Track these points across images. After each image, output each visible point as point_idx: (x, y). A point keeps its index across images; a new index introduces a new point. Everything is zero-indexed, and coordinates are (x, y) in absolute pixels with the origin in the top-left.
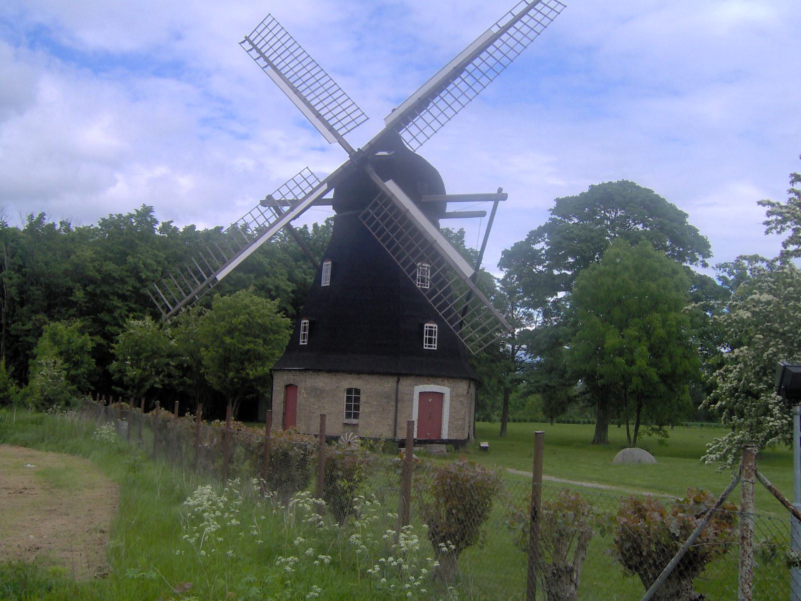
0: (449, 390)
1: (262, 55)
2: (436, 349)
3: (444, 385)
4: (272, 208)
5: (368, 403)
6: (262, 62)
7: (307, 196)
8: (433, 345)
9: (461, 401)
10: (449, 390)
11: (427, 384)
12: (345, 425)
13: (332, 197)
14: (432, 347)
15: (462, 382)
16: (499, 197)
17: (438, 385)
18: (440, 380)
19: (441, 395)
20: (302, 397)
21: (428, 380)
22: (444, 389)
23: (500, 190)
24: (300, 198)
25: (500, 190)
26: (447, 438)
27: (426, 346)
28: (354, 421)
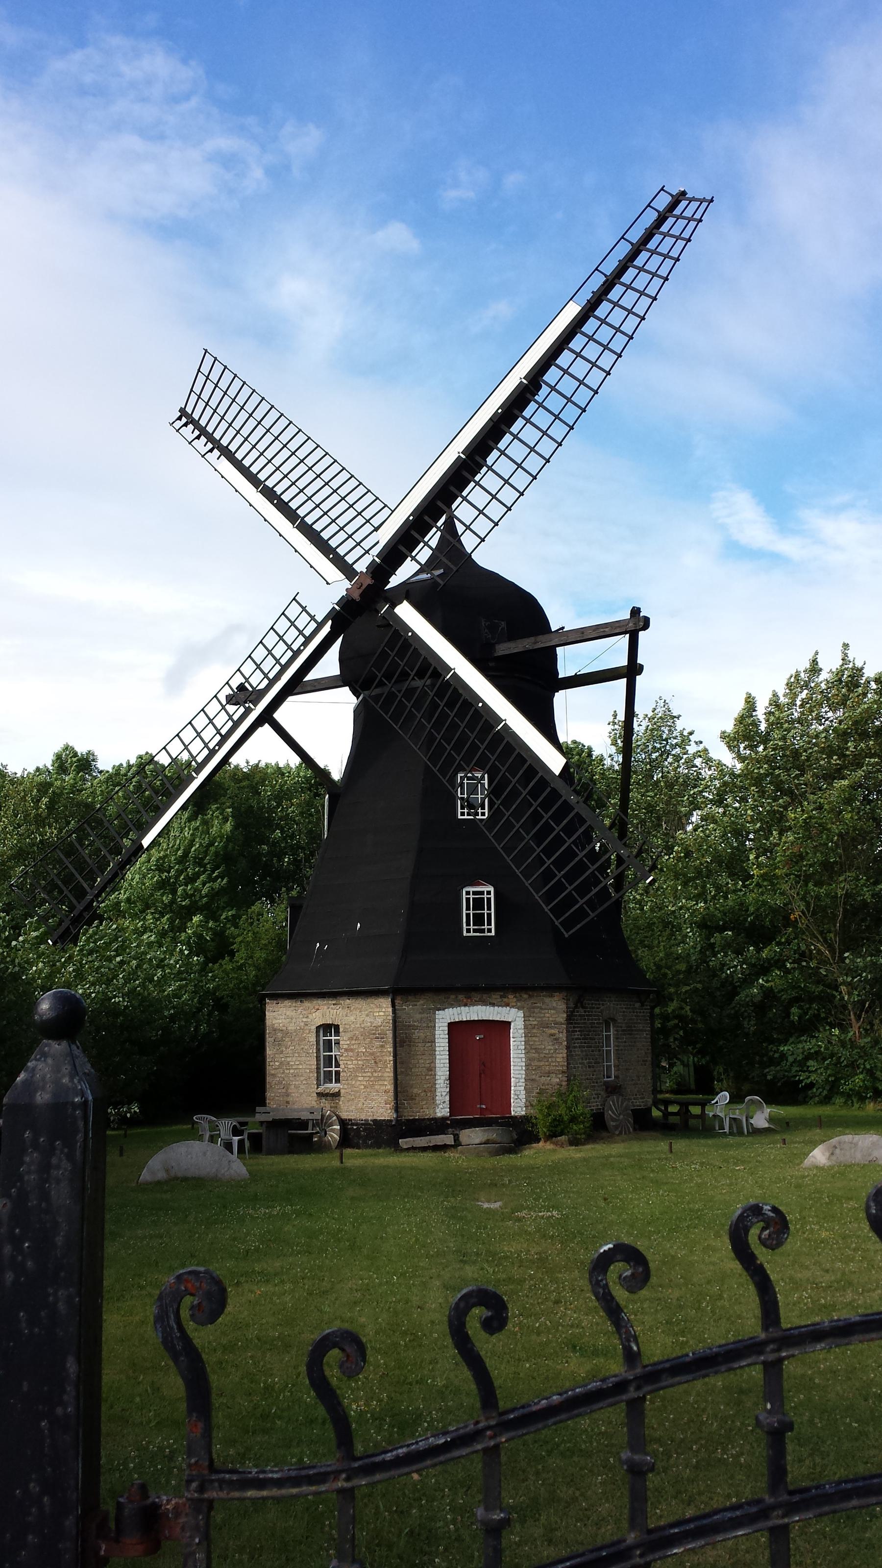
0: (521, 1014)
1: (203, 432)
2: (465, 934)
3: (507, 1005)
4: (250, 689)
5: (352, 1050)
6: (202, 444)
7: (272, 683)
8: (472, 927)
9: (552, 1035)
10: (521, 1014)
11: (465, 1005)
12: (320, 1095)
13: (337, 672)
14: (483, 931)
15: (552, 996)
16: (636, 625)
17: (493, 1005)
18: (496, 997)
19: (505, 1025)
20: (797, 1542)
21: (469, 998)
22: (513, 1016)
23: (635, 612)
24: (262, 686)
25: (635, 612)
26: (523, 1113)
27: (468, 931)
28: (333, 1087)
